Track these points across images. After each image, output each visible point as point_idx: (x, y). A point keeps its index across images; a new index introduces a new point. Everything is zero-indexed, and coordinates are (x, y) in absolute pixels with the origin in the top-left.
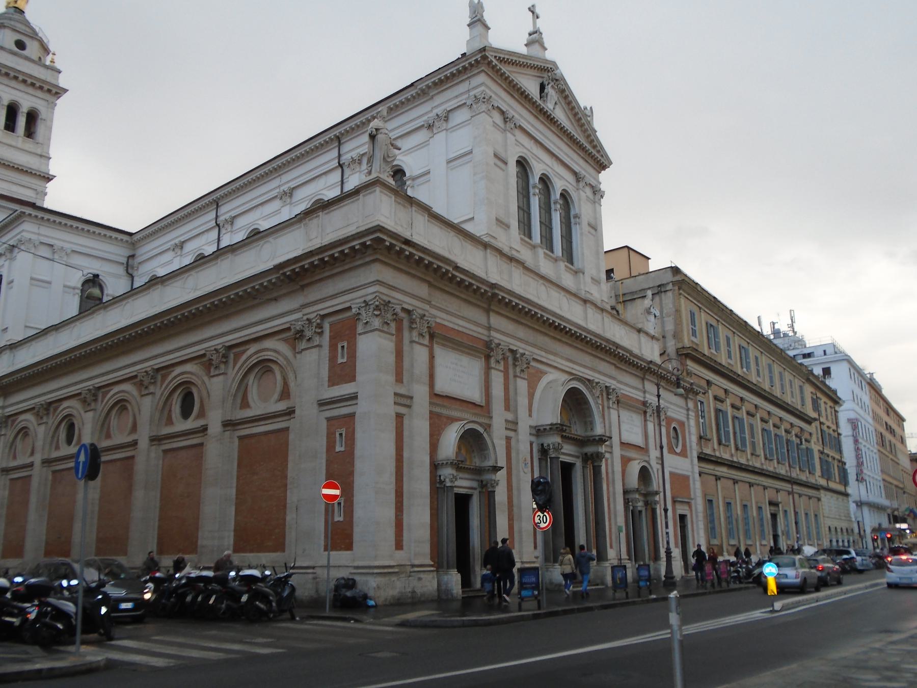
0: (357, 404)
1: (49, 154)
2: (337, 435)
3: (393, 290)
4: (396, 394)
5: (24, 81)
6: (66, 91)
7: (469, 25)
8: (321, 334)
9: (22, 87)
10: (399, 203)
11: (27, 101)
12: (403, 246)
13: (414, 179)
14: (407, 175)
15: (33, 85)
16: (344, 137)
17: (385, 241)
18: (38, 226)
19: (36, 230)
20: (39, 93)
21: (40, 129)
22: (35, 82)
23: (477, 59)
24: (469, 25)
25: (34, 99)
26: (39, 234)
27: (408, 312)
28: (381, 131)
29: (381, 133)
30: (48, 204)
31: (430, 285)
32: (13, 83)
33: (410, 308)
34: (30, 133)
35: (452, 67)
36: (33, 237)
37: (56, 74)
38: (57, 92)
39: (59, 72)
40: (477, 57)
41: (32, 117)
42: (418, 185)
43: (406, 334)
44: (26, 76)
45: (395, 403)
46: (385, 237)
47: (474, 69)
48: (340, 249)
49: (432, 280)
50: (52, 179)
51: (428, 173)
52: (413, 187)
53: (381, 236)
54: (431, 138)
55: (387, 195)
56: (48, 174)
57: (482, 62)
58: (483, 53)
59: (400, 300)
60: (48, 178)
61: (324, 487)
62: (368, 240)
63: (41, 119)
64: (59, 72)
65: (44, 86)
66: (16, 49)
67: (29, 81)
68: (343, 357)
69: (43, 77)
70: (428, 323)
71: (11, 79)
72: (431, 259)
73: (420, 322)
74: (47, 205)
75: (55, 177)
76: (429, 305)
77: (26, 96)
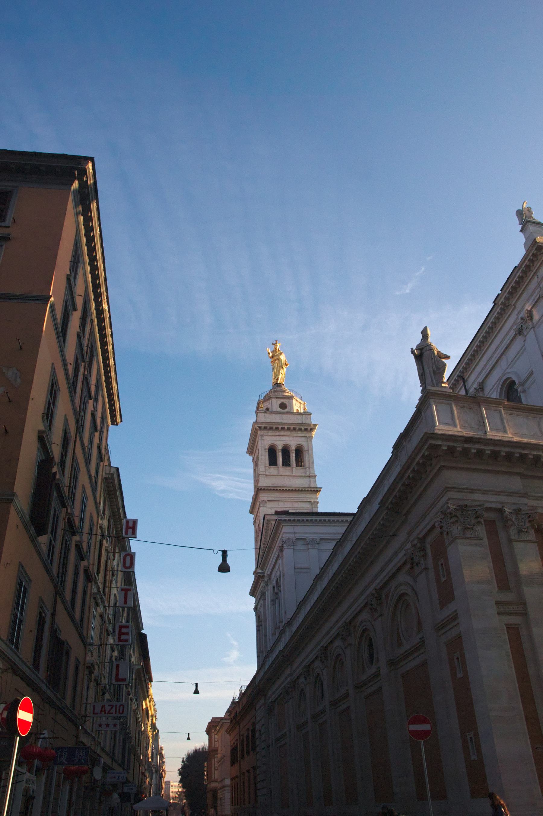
0: (458, 623)
1: (314, 473)
2: (456, 660)
3: (469, 492)
4: (497, 603)
5: (289, 429)
6: (315, 425)
7: (521, 231)
8: (425, 556)
9: (288, 433)
10: (464, 407)
11: (293, 442)
12: (466, 445)
13: (522, 384)
14: (517, 382)
15: (294, 429)
16: (465, 374)
17: (440, 446)
18: (292, 527)
19: (292, 531)
20: (300, 434)
21: (306, 458)
22: (283, 426)
23: (533, 253)
24: (521, 231)
25: (296, 439)
26: (295, 533)
27: (500, 511)
28: (425, 349)
29: (426, 351)
30: (321, 509)
31: (522, 476)
32: (282, 433)
33: (500, 506)
34: (300, 462)
35: (517, 272)
36: (292, 536)
37: (308, 416)
38: (309, 429)
39: (310, 414)
40: (533, 252)
41: (299, 451)
42: (528, 389)
43: (502, 535)
44: (260, 424)
45: (499, 614)
46: (440, 443)
47: (536, 263)
48: (411, 469)
49: (522, 471)
50: (320, 491)
51: (532, 373)
52: (524, 391)
53: (434, 442)
54: (524, 341)
55: (443, 403)
56: (317, 488)
57: (539, 253)
58: (536, 245)
59: (480, 501)
60: (317, 491)
61: (409, 723)
62: (424, 451)
63: (305, 451)
64: (310, 414)
65: (279, 426)
66: (280, 410)
67: (292, 427)
68: (444, 576)
69: (278, 421)
70: (529, 517)
71: (292, 431)
72: (507, 449)
73: (516, 519)
74: (320, 510)
75: (321, 488)
76: (525, 497)
77: (291, 438)
